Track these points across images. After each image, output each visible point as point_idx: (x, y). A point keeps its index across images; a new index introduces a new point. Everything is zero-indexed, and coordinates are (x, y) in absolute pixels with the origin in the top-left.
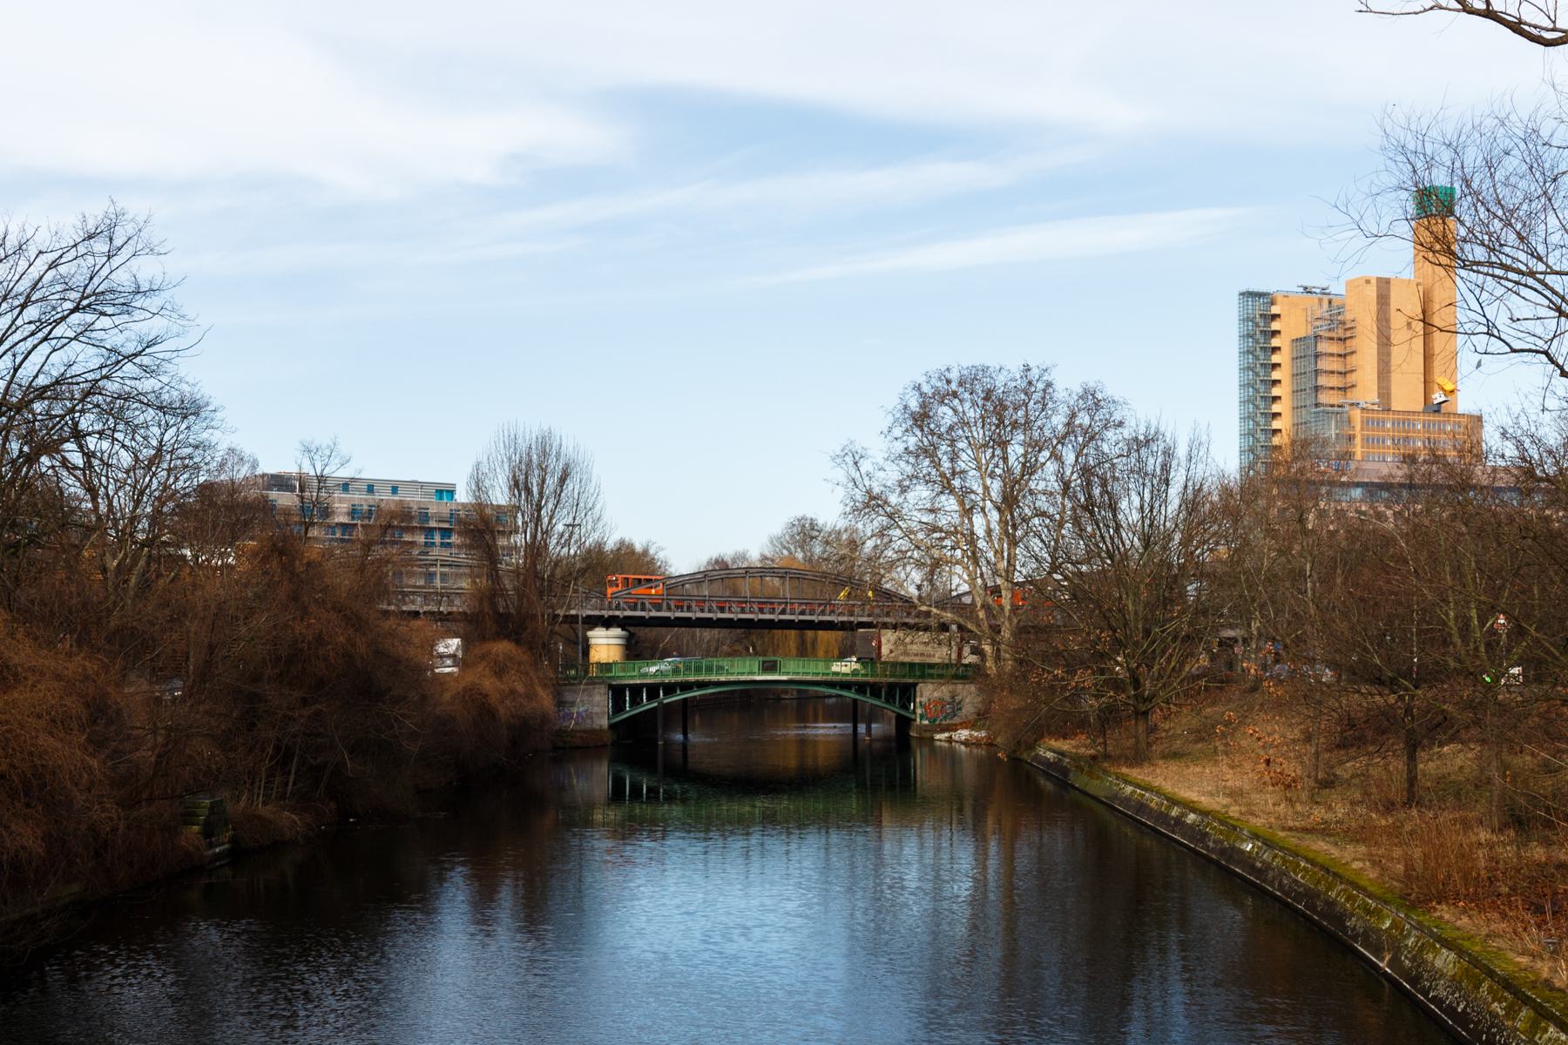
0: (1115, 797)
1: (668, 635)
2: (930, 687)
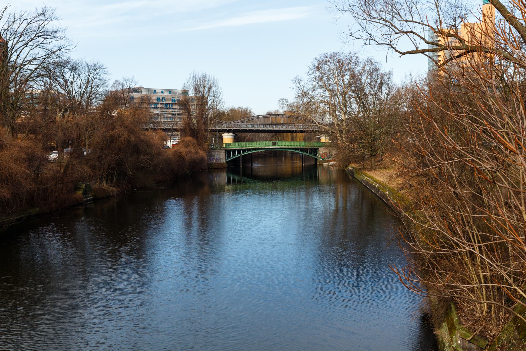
0: (363, 180)
1: (249, 135)
2: (323, 149)
